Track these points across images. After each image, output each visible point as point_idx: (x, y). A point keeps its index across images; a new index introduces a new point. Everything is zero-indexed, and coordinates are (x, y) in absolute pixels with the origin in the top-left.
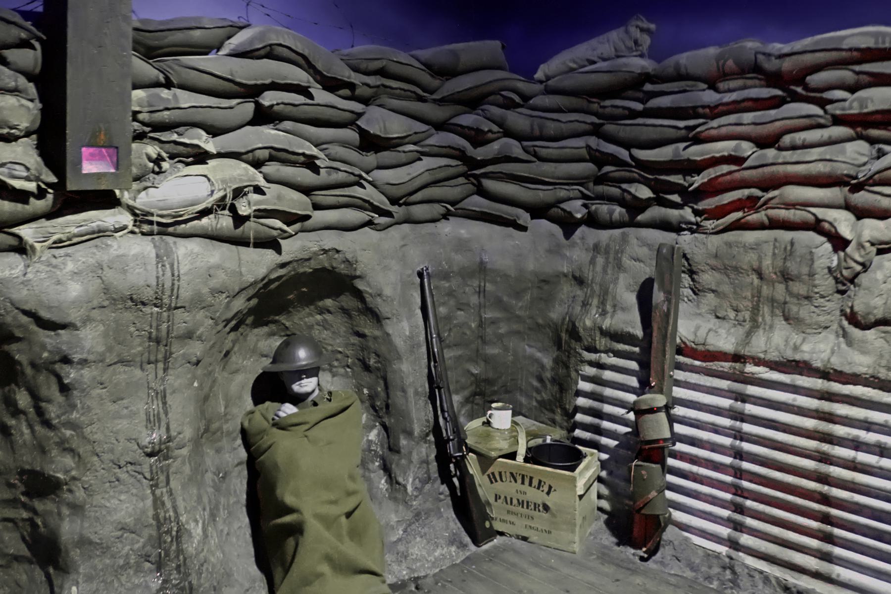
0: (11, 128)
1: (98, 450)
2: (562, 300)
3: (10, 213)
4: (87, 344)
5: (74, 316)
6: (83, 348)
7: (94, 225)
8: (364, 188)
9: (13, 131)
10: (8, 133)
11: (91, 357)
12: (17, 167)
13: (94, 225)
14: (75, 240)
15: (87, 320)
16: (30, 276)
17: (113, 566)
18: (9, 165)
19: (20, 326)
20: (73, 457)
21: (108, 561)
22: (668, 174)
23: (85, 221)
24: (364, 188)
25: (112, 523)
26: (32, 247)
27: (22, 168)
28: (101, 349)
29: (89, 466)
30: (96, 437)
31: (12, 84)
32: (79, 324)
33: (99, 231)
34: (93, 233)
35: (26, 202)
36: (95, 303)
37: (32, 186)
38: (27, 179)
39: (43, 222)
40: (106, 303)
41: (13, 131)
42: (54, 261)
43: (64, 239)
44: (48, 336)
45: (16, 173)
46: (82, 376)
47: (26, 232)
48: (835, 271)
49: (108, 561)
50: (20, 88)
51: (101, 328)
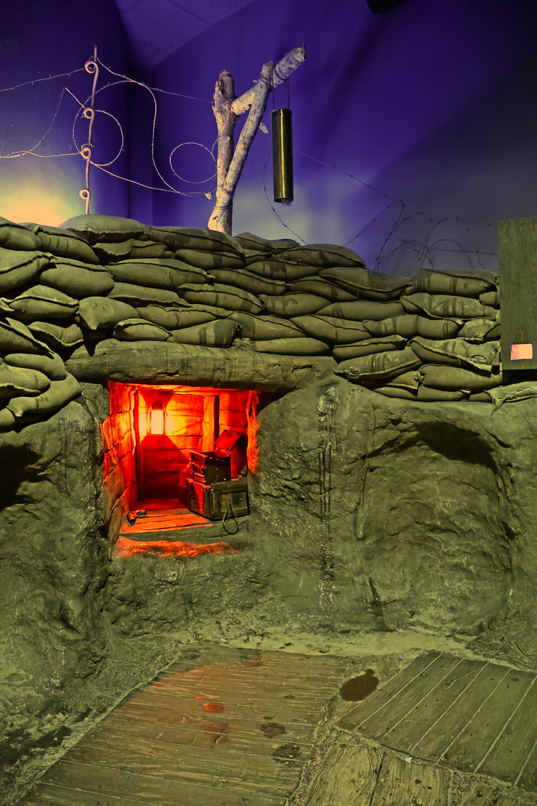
0: (475, 337)
1: (531, 522)
2: (195, 429)
3: (483, 382)
4: (520, 458)
5: (512, 441)
6: (517, 460)
7: (526, 390)
8: (52, 358)
9: (476, 339)
10: (474, 340)
11: (522, 466)
12: (480, 357)
13: (526, 390)
14: (518, 398)
15: (519, 445)
16: (494, 416)
17: (532, 589)
18: (476, 357)
19: (492, 443)
20: (519, 522)
21: (530, 585)
22: (41, 341)
23: (521, 387)
24: (52, 358)
25: (534, 565)
26: (495, 400)
27: (483, 358)
28: (528, 463)
29: (526, 529)
30: (530, 513)
31: (482, 313)
32: (514, 446)
33: (530, 394)
34: (527, 395)
35: (489, 376)
36: (525, 435)
37: (489, 368)
38: (487, 364)
39: (501, 388)
40: (532, 437)
41: (476, 339)
42: (507, 409)
43: (511, 397)
44: (503, 450)
45: (481, 361)
46: (518, 475)
47: (493, 392)
48: (275, 438)
49: (530, 585)
50: (486, 314)
51: (529, 451)
